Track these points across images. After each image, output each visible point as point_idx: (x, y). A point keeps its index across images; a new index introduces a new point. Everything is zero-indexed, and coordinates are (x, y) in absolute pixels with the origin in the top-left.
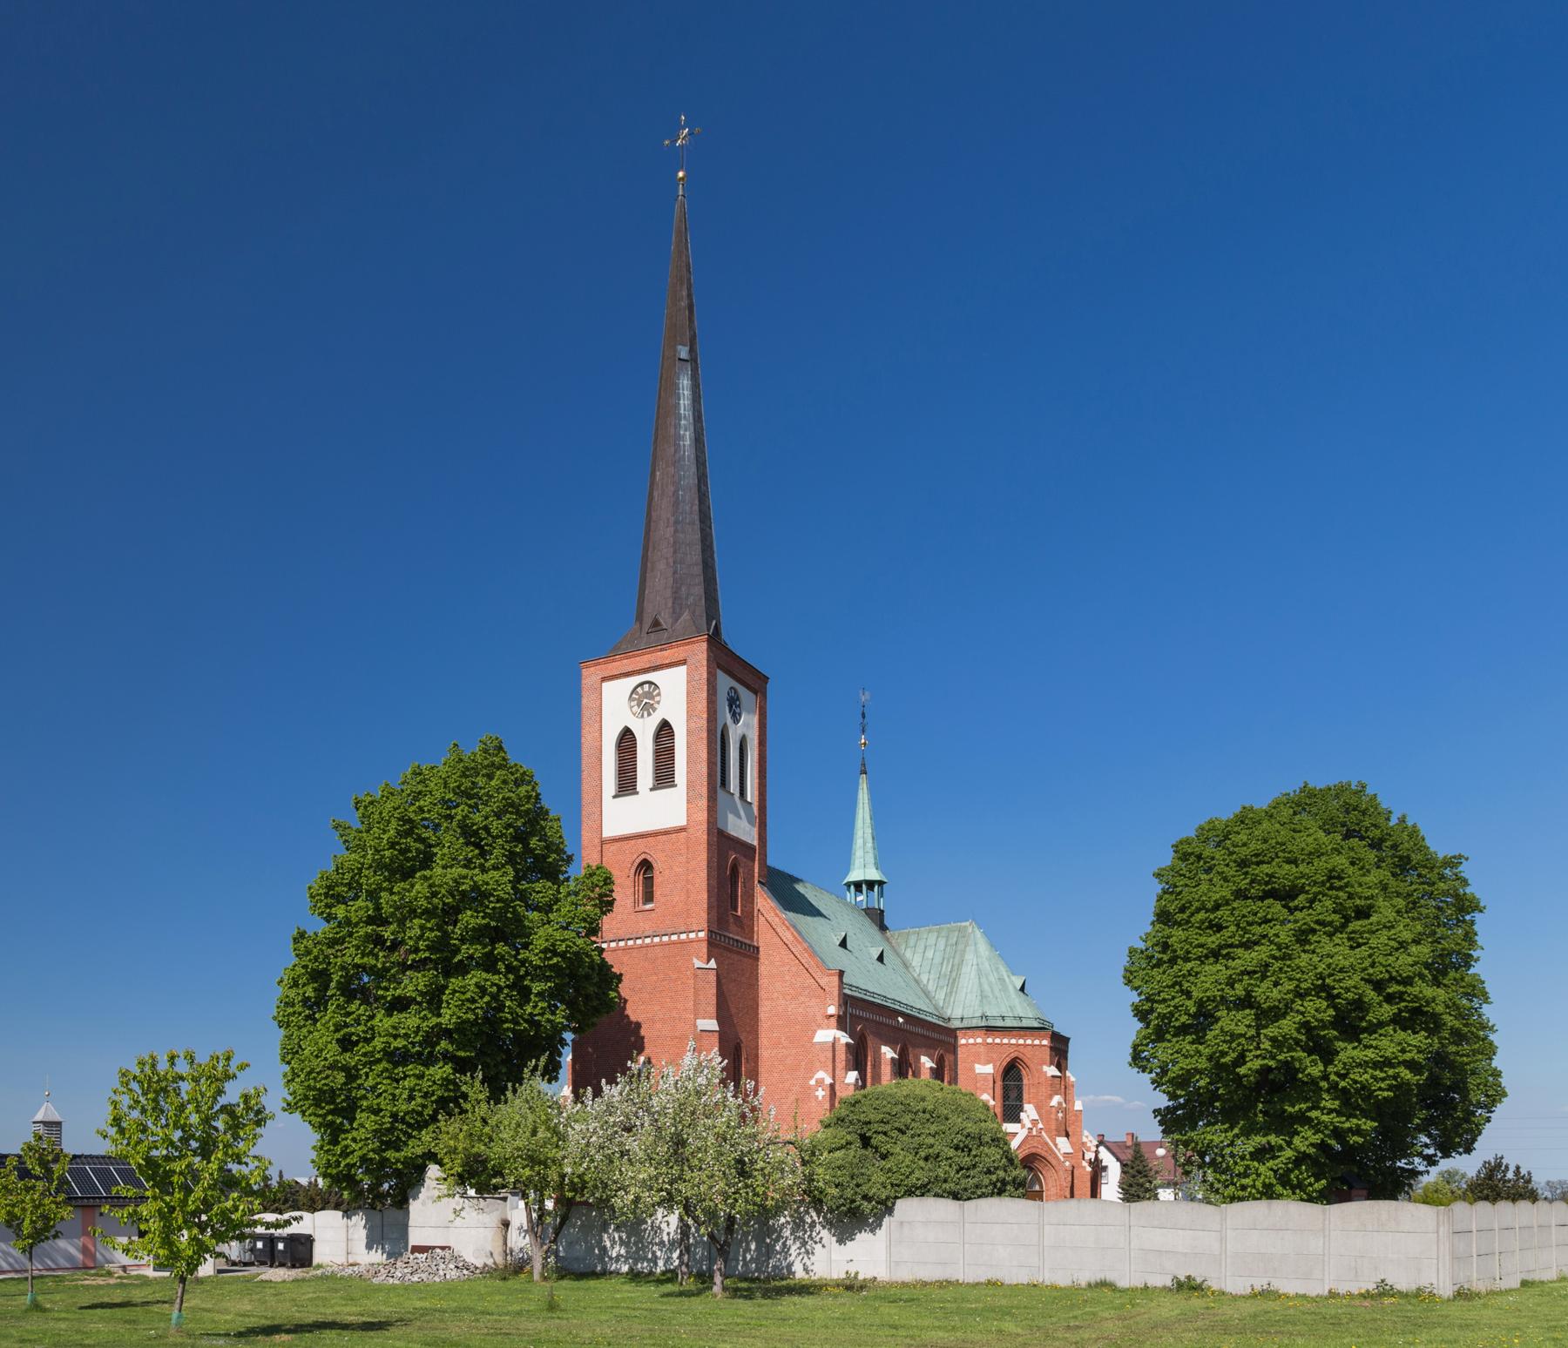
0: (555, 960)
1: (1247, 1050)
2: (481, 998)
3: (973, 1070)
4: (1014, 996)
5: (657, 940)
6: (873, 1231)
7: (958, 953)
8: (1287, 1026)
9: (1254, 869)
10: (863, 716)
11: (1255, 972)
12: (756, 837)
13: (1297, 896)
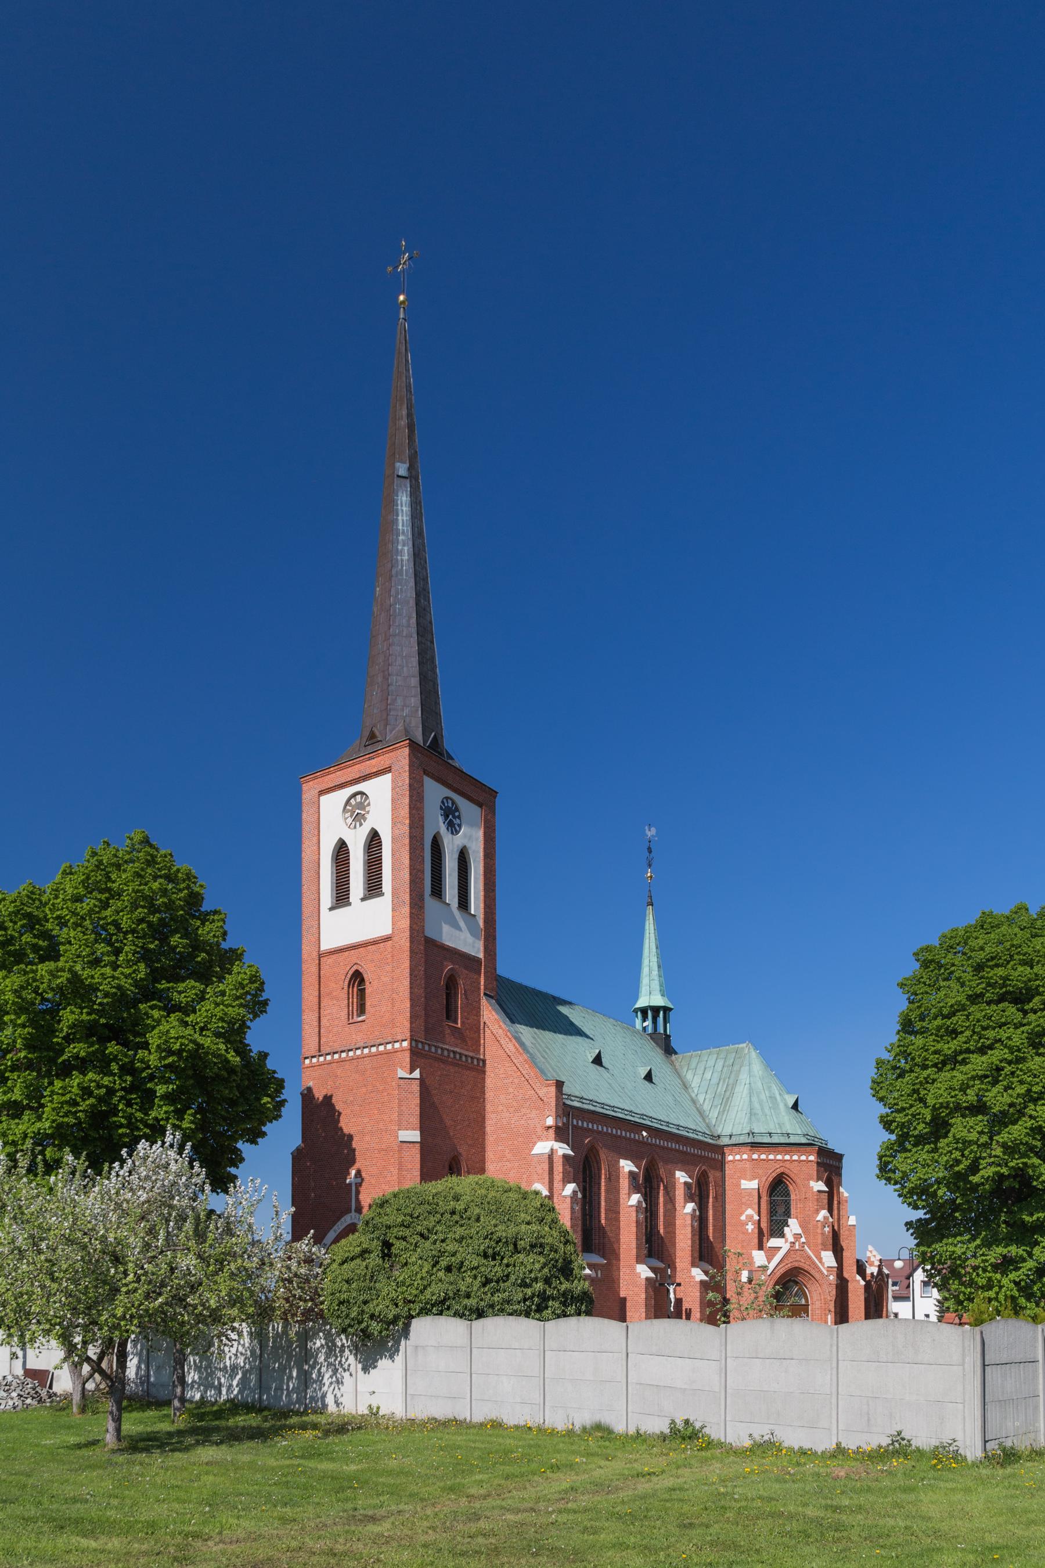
0: (170, 1060)
1: (980, 1158)
2: (84, 1100)
4: (784, 1114)
5: (366, 1051)
6: (391, 1357)
7: (733, 1073)
8: (1017, 1131)
9: (987, 973)
10: (650, 850)
11: (986, 1077)
12: (482, 948)
13: (1033, 997)
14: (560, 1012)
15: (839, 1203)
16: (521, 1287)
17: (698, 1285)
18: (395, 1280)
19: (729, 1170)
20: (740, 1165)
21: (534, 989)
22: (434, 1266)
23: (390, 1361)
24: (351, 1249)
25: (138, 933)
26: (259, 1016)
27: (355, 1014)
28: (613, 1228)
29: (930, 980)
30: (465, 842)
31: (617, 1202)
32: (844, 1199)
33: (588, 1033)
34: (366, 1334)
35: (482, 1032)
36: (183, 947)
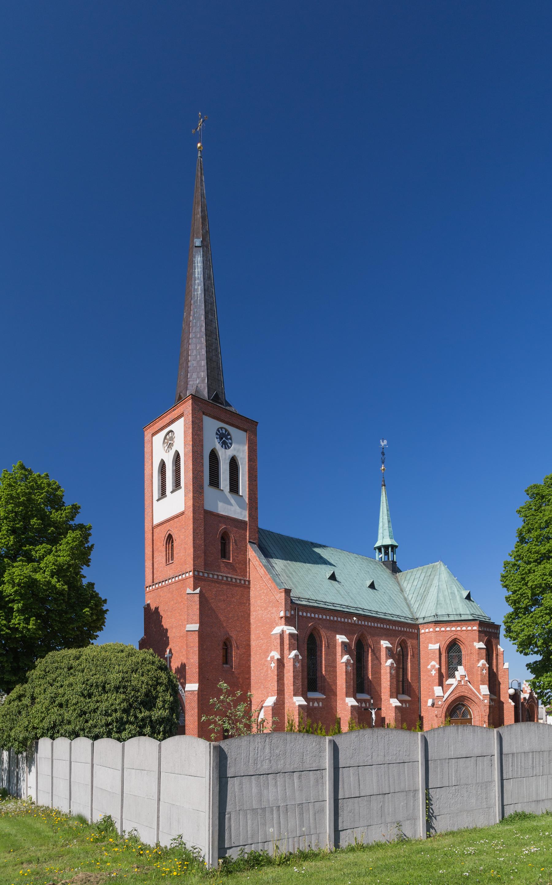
4: (459, 602)
7: (430, 580)
10: (383, 454)
12: (247, 515)
15: (497, 655)
17: (394, 709)
20: (429, 635)
21: (288, 537)
25: (9, 518)
28: (331, 677)
30: (235, 453)
31: (334, 661)
32: (501, 652)
33: (332, 562)
35: (248, 564)
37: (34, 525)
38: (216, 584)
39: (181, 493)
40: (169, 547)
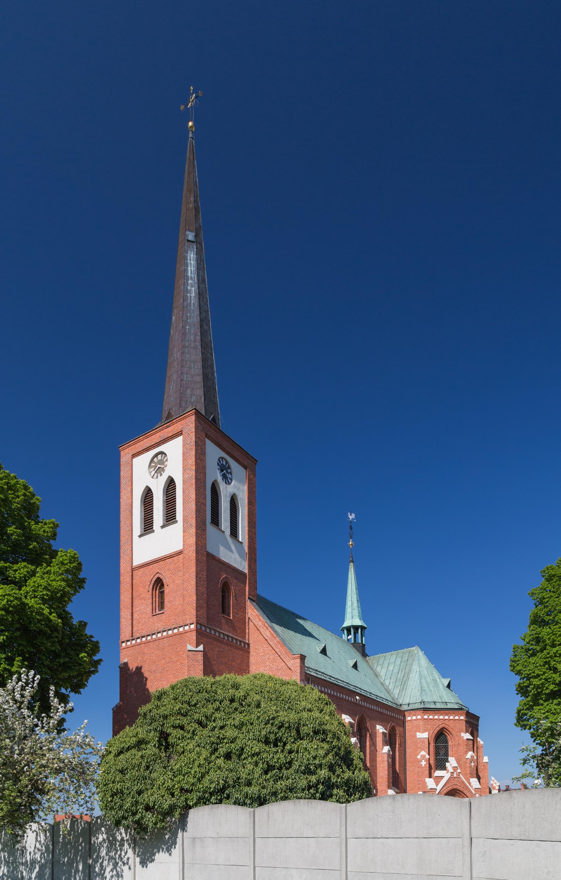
3: (415, 736)
4: (442, 690)
5: (165, 634)
6: (169, 850)
7: (408, 666)
12: (247, 567)
14: (298, 622)
15: (477, 748)
16: (304, 774)
18: (172, 769)
19: (408, 726)
22: (212, 753)
23: (167, 854)
24: (128, 739)
26: (78, 592)
27: (157, 609)
29: (554, 588)
30: (235, 491)
32: (480, 745)
34: (140, 827)
35: (247, 624)
36: (18, 536)
37: (12, 535)
38: (218, 643)
39: (177, 529)
40: (156, 594)
